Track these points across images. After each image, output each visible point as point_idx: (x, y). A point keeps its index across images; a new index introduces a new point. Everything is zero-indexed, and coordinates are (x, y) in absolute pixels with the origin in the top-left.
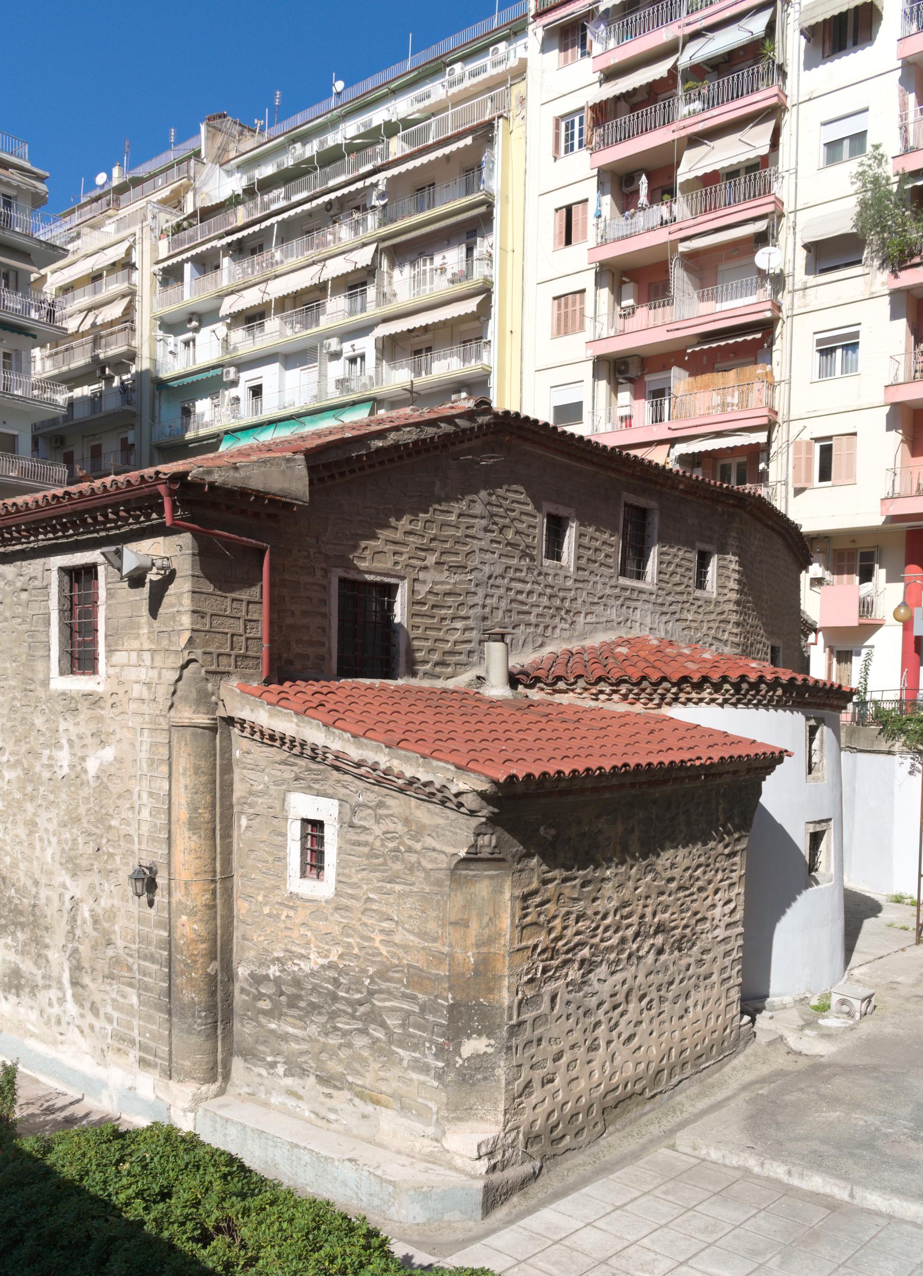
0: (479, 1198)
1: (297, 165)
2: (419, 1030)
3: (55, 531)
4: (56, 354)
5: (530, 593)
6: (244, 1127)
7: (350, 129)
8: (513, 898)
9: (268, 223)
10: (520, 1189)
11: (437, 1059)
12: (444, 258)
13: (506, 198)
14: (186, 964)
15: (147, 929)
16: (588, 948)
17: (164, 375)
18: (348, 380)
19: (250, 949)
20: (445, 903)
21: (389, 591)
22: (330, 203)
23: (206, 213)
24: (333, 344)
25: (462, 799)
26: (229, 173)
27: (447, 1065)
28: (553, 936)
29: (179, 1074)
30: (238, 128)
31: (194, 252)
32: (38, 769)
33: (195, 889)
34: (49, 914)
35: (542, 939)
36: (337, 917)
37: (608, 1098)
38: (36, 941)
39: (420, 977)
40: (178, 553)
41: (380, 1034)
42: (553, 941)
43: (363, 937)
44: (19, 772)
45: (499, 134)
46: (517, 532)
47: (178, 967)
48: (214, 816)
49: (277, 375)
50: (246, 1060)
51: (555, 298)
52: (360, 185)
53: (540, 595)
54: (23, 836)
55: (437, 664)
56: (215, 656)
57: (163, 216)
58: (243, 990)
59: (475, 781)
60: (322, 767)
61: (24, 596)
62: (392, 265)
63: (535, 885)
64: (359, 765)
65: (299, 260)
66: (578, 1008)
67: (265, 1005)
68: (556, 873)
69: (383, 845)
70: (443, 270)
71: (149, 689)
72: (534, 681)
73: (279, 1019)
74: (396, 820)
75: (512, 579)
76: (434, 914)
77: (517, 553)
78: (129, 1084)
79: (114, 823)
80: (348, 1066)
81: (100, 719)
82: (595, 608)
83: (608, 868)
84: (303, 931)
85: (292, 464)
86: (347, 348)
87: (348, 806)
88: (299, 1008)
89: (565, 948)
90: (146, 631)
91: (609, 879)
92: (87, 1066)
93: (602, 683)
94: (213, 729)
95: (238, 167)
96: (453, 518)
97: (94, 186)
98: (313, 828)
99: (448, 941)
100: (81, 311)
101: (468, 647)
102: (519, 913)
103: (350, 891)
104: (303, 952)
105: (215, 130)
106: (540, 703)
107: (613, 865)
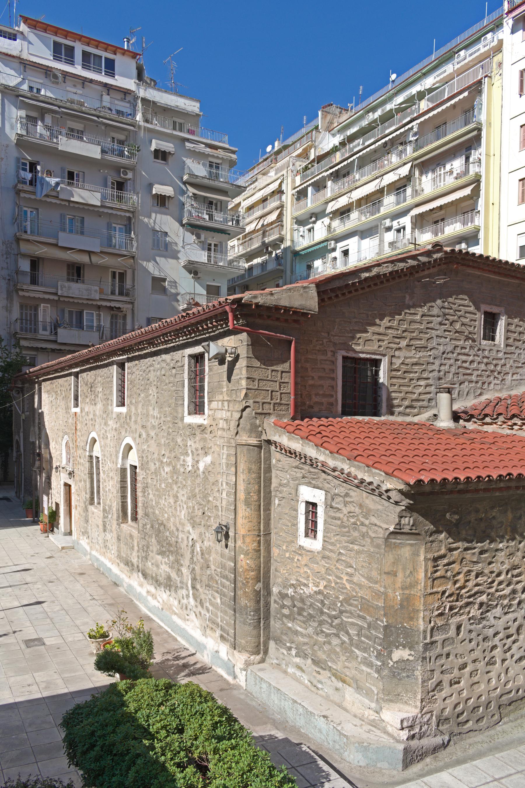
0: (401, 756)
1: (369, 124)
2: (367, 639)
3: (186, 335)
4: (245, 242)
5: (472, 362)
6: (270, 685)
7: (400, 99)
8: (426, 559)
9: (352, 159)
10: (432, 754)
11: (377, 660)
12: (452, 165)
13: (489, 124)
14: (243, 583)
15: (225, 561)
16: (485, 595)
17: (298, 248)
18: (396, 242)
19: (279, 577)
20: (382, 560)
21: (377, 363)
22: (386, 143)
23: (320, 159)
24: (388, 222)
25: (390, 494)
26: (334, 135)
27: (383, 664)
28: (457, 585)
29: (239, 648)
30: (339, 110)
31: (313, 181)
32: (178, 466)
33: (248, 540)
34: (183, 547)
35: (449, 587)
36: (323, 562)
37: (503, 698)
38: (177, 561)
39: (368, 605)
40: (240, 345)
41: (346, 639)
42: (457, 589)
43: (337, 577)
44: (171, 467)
45: (485, 88)
46: (463, 324)
47: (239, 585)
48: (260, 498)
49: (357, 243)
50: (276, 643)
51: (520, 180)
52: (402, 130)
53: (479, 363)
54: (172, 504)
55: (407, 407)
56: (261, 404)
57: (298, 164)
58: (275, 601)
59: (396, 483)
60: (316, 471)
61: (174, 371)
62: (421, 174)
63: (443, 551)
64: (334, 470)
65: (370, 177)
66: (478, 635)
67: (286, 611)
68: (460, 544)
69: (348, 520)
70: (451, 172)
71: (227, 423)
72: (470, 417)
73: (293, 621)
74: (355, 505)
75: (459, 354)
76: (376, 566)
77: (463, 338)
78: (216, 649)
79: (211, 499)
80: (329, 656)
81: (204, 440)
82: (518, 370)
83: (500, 543)
84: (306, 569)
85: (307, 290)
86: (395, 224)
87: (329, 495)
88: (303, 616)
89: (467, 594)
90: (225, 390)
91: (501, 550)
92: (197, 634)
93: (515, 419)
94: (260, 447)
95: (339, 131)
96: (418, 317)
97: (266, 153)
98: (312, 506)
99: (383, 584)
100: (257, 219)
101: (428, 396)
102: (430, 570)
103: (330, 547)
104: (306, 582)
105: (326, 113)
106: (472, 431)
107: (505, 541)
